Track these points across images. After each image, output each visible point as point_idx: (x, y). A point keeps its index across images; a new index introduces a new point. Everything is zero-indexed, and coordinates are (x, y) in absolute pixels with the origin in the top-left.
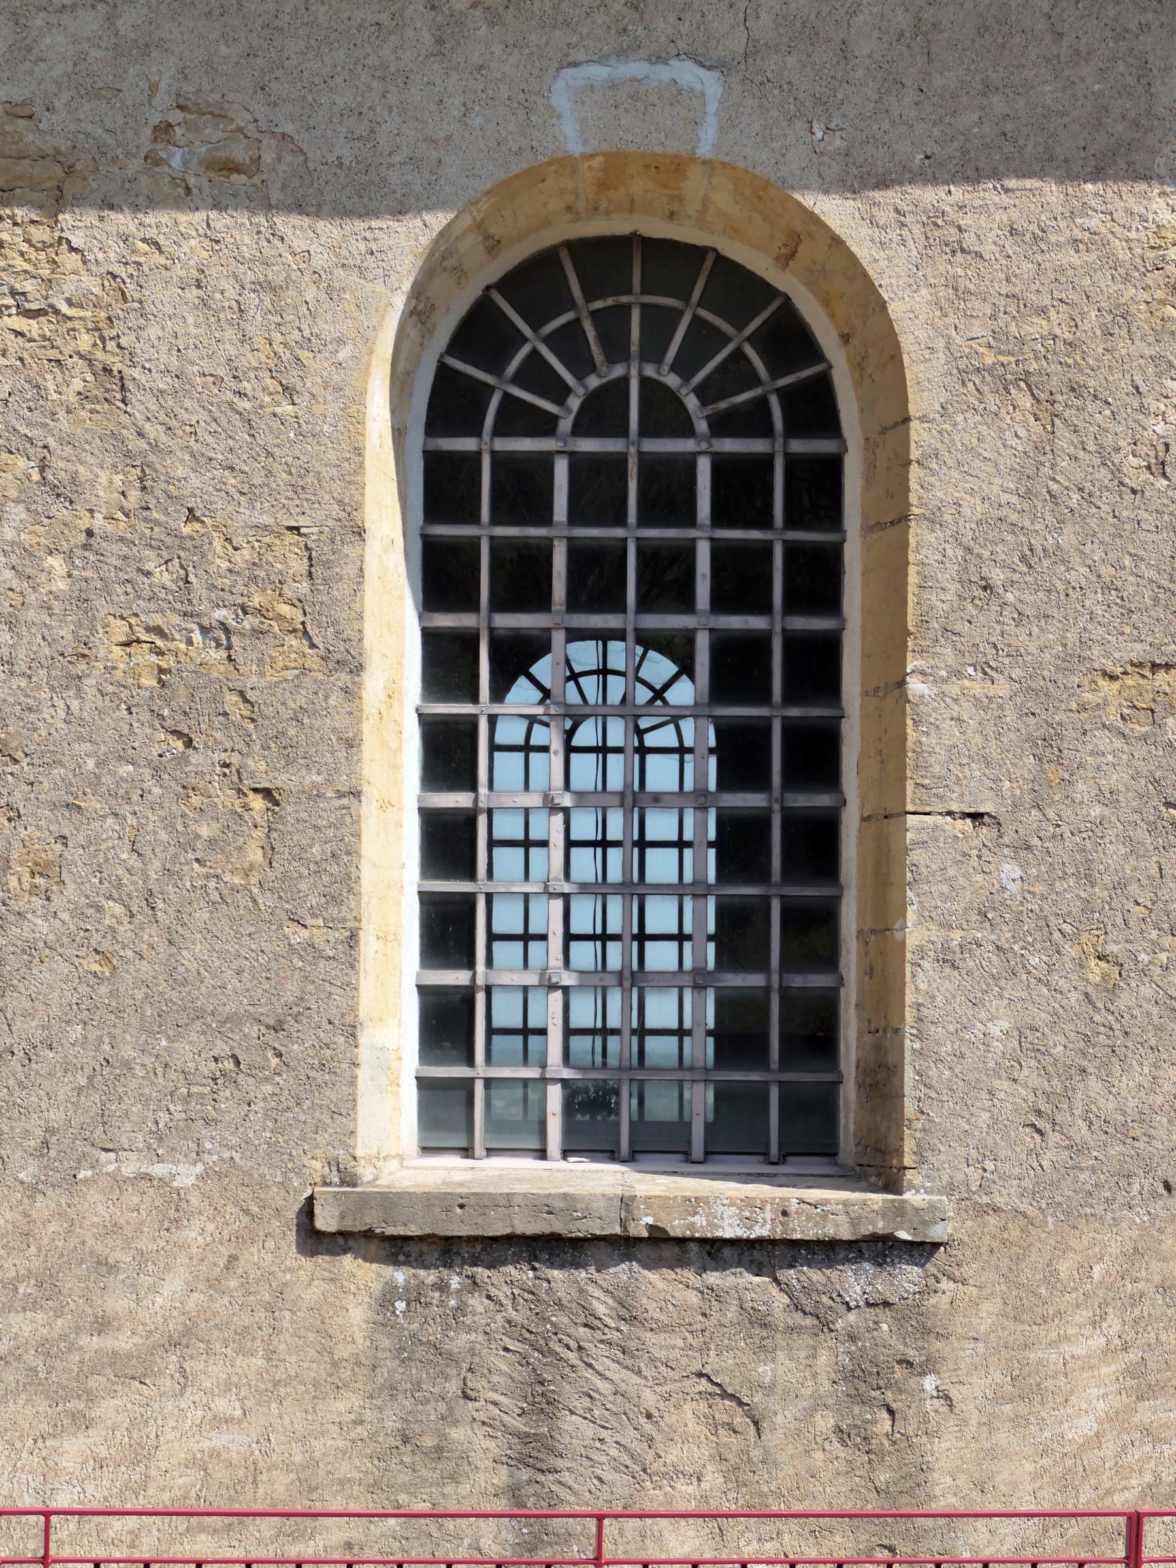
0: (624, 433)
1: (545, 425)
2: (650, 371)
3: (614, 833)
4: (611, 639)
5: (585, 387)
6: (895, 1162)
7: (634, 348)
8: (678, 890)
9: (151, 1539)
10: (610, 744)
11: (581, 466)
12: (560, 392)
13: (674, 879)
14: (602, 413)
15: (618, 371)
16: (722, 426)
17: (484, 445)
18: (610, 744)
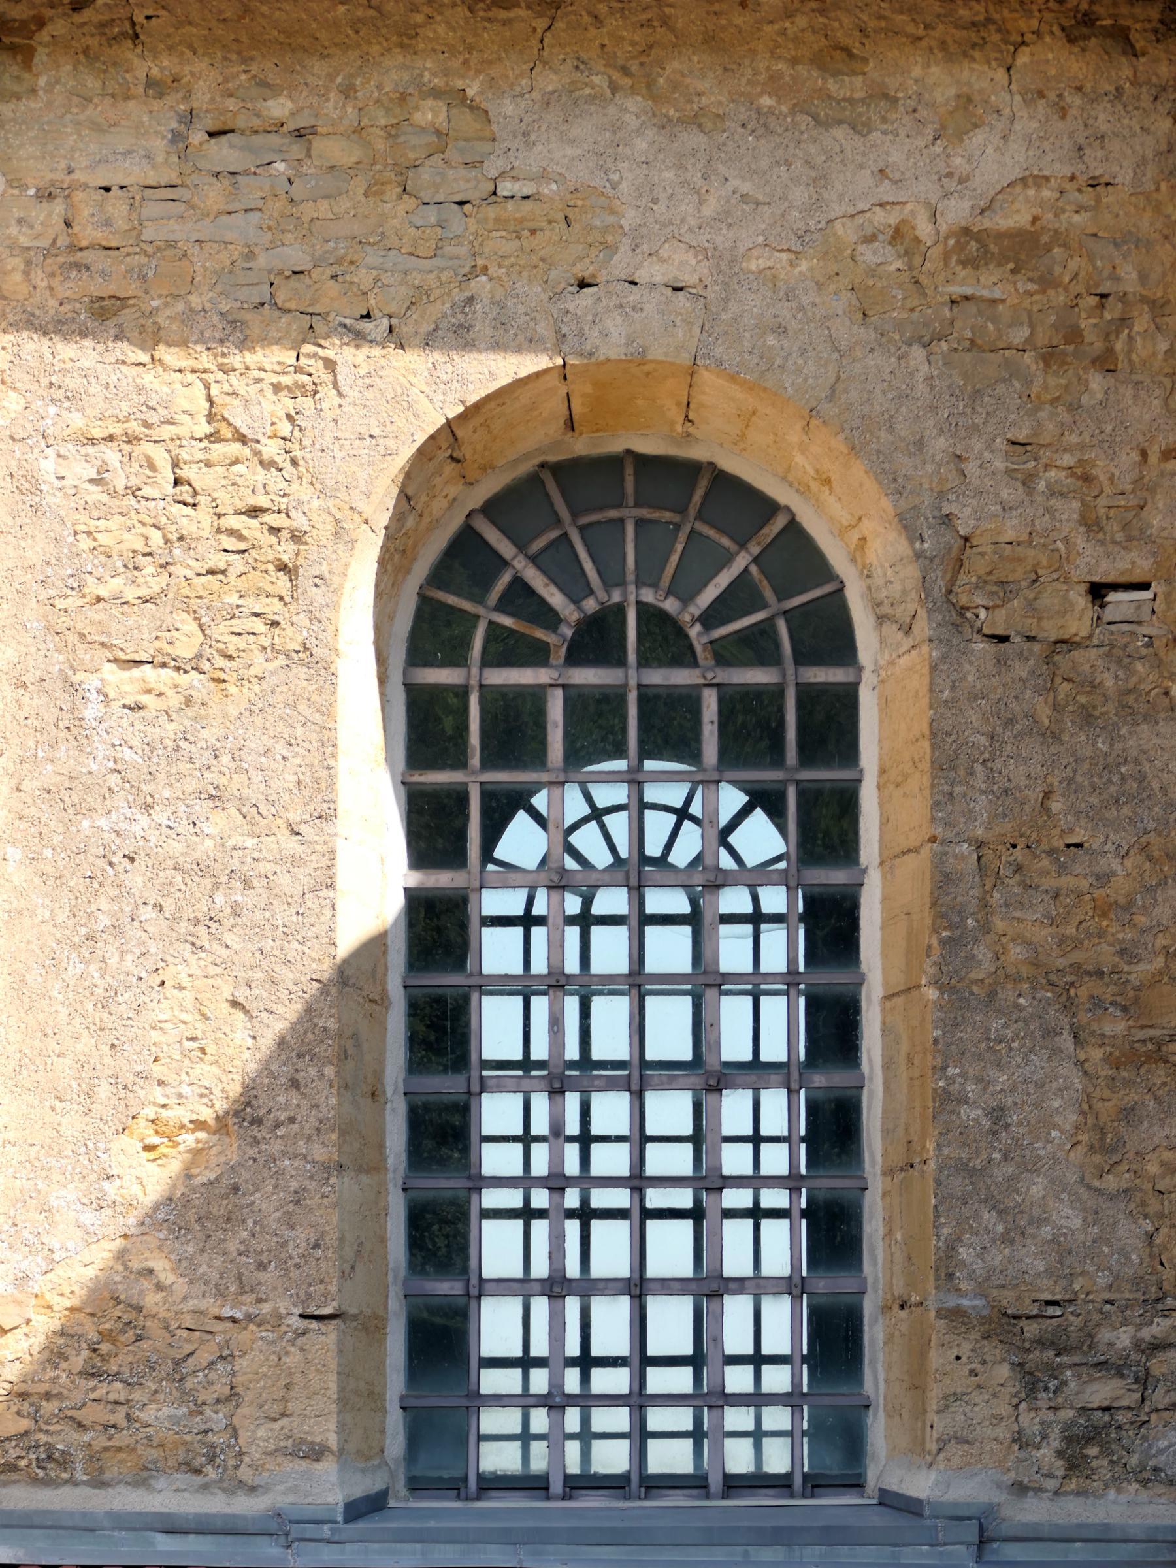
0: (622, 662)
1: (538, 655)
2: (648, 596)
3: (539, 909)
4: (612, 865)
5: (580, 609)
6: (422, 844)
7: (631, 577)
8: (755, 987)
9: (166, 1547)
10: (766, 1350)
11: (576, 700)
12: (548, 617)
13: (519, 1273)
14: (597, 640)
15: (616, 597)
16: (724, 654)
17: (475, 677)
18: (766, 1350)
